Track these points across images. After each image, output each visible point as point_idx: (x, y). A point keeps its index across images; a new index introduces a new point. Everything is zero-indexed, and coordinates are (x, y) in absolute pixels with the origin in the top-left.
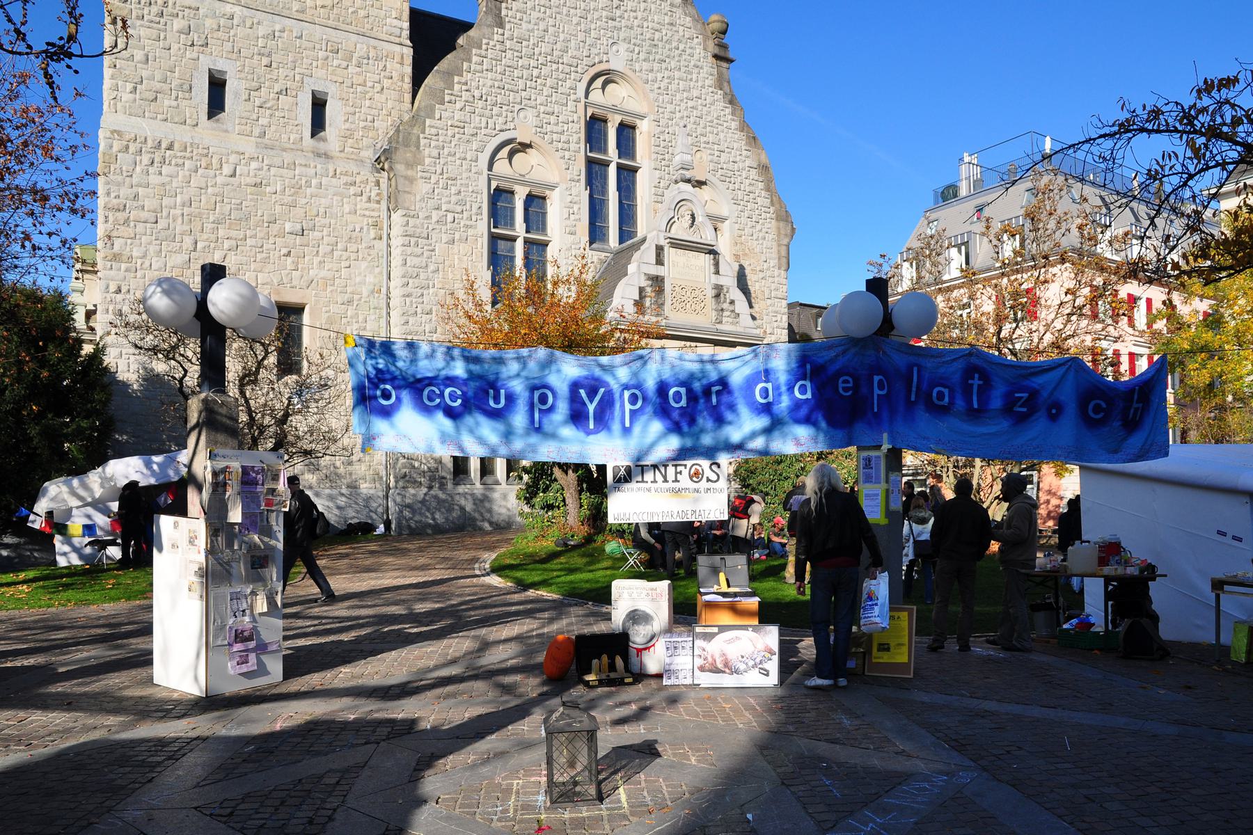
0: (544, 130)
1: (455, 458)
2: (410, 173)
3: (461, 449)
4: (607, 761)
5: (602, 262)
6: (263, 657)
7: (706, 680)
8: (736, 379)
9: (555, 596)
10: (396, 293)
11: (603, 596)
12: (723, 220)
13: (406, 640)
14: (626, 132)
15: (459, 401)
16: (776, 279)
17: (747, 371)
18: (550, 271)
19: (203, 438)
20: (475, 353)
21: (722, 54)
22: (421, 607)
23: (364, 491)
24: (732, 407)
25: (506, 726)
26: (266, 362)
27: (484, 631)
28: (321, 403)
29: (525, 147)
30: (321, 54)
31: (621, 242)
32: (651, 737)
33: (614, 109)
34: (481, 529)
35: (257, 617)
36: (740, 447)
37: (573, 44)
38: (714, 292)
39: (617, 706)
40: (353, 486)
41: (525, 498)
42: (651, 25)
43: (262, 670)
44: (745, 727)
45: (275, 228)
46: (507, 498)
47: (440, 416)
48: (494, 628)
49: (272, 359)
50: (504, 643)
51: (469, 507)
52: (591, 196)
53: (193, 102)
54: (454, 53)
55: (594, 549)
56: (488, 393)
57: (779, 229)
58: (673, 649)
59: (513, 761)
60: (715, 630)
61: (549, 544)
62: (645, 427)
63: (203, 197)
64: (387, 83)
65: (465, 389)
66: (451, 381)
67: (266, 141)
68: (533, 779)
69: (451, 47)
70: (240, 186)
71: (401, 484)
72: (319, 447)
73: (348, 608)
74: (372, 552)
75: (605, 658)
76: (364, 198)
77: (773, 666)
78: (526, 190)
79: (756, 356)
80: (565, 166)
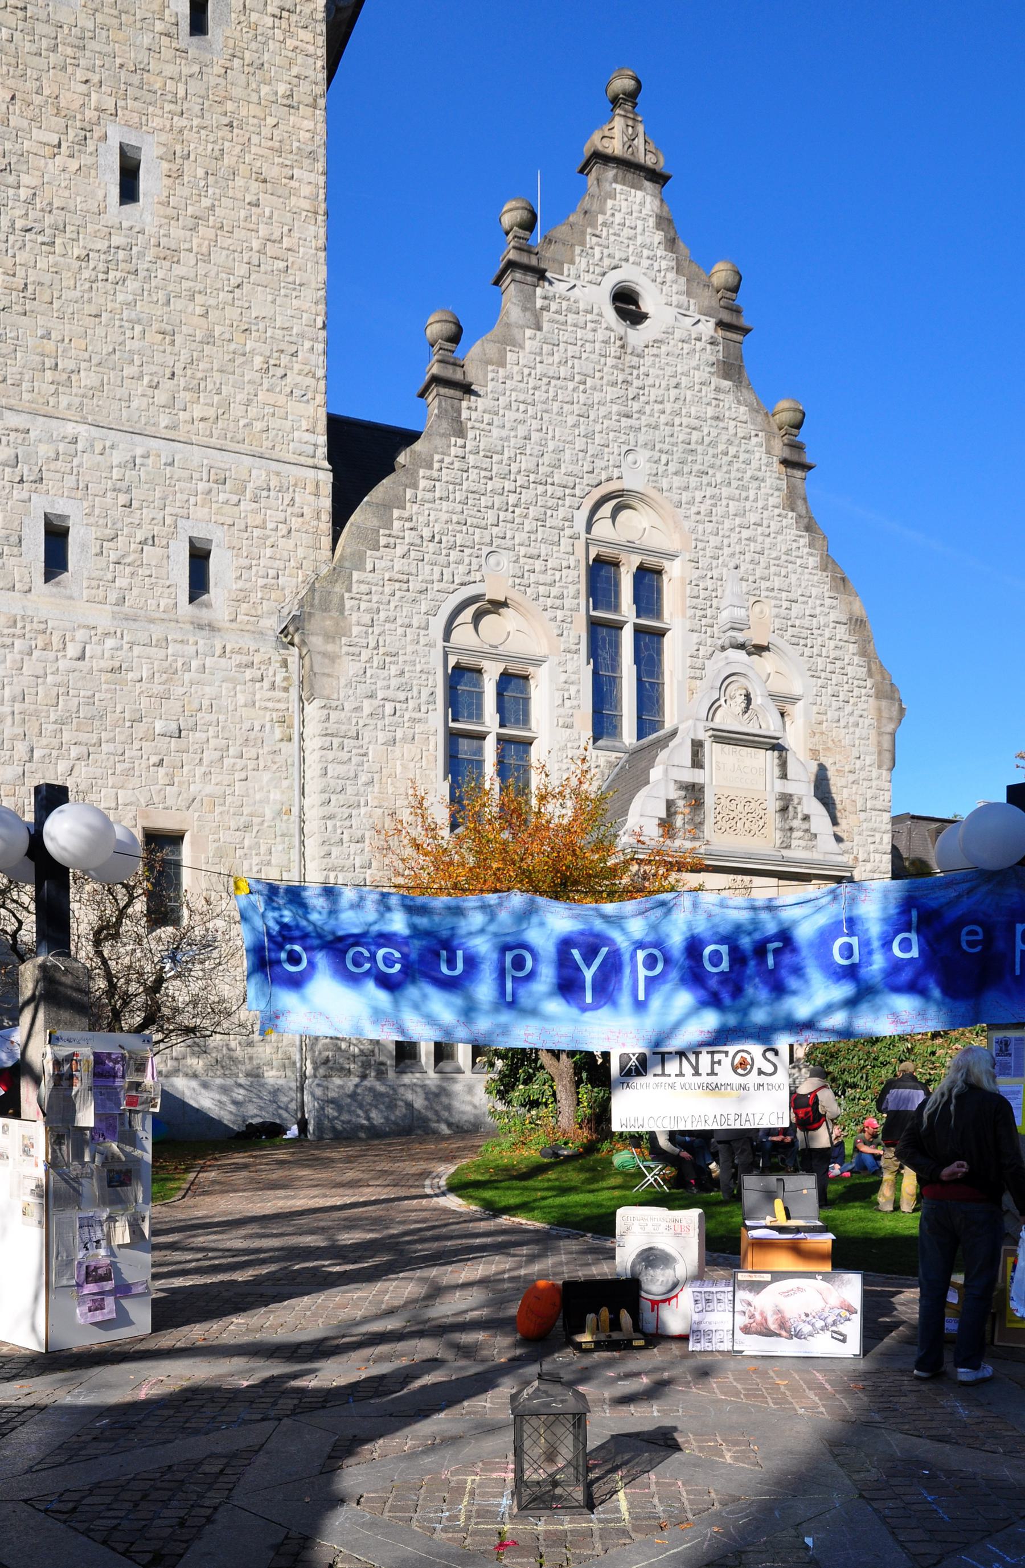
0: (525, 581)
1: (398, 1044)
2: (330, 648)
3: (402, 1030)
4: (603, 1453)
5: (611, 765)
6: (124, 1302)
7: (752, 1345)
8: (805, 932)
9: (539, 1225)
10: (313, 814)
11: (604, 1226)
12: (794, 700)
13: (323, 1282)
14: (648, 579)
15: (398, 967)
16: (874, 783)
17: (822, 920)
18: (536, 780)
19: (41, 1016)
20: (420, 900)
21: (795, 458)
22: (348, 1238)
23: (271, 1081)
24: (798, 971)
25: (460, 1401)
26: (130, 911)
27: (434, 1272)
28: (208, 965)
29: (497, 606)
30: (202, 486)
31: (639, 738)
32: (668, 1422)
33: (631, 548)
34: (435, 1132)
35: (116, 1250)
36: (809, 1025)
37: (567, 455)
38: (779, 805)
39: (620, 1378)
40: (255, 1075)
41: (499, 1092)
42: (685, 421)
43: (123, 1319)
44: (809, 1416)
45: (140, 729)
46: (473, 1092)
47: (370, 986)
48: (449, 1268)
49: (139, 906)
50: (464, 1289)
51: (419, 1102)
52: (595, 673)
53: (24, 560)
54: (392, 476)
55: (596, 1161)
56: (438, 955)
57: (879, 710)
58: (706, 1302)
59: (468, 1450)
60: (767, 1277)
61: (531, 1154)
62: (668, 999)
63: (40, 689)
64: (295, 523)
65: (405, 950)
66: (386, 939)
67: (126, 609)
68: (495, 1475)
69: (389, 469)
70: (91, 672)
71: (322, 1071)
72: (206, 1023)
73: (245, 1237)
74: (282, 1163)
75: (605, 1312)
76: (266, 684)
77: (853, 1329)
78: (500, 667)
79: (835, 898)
80: (556, 632)
